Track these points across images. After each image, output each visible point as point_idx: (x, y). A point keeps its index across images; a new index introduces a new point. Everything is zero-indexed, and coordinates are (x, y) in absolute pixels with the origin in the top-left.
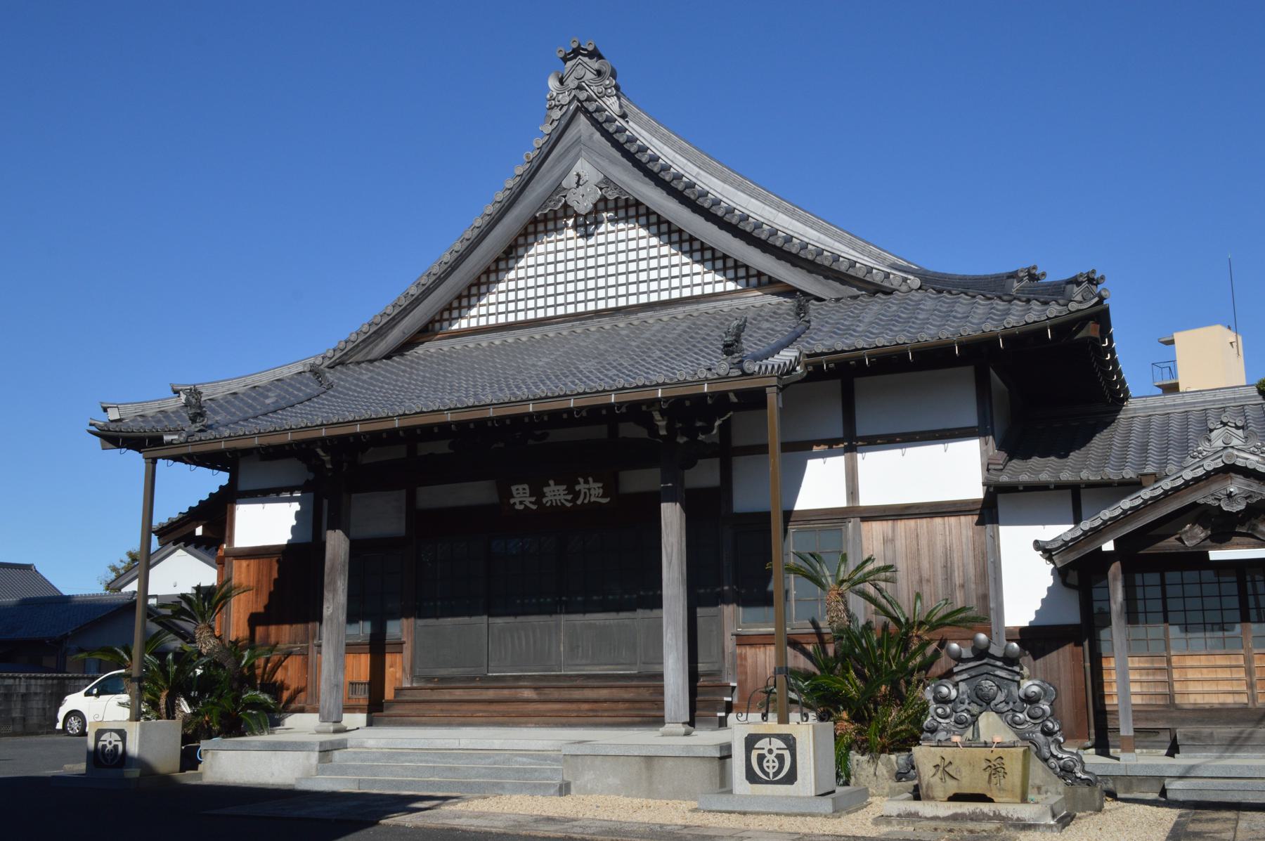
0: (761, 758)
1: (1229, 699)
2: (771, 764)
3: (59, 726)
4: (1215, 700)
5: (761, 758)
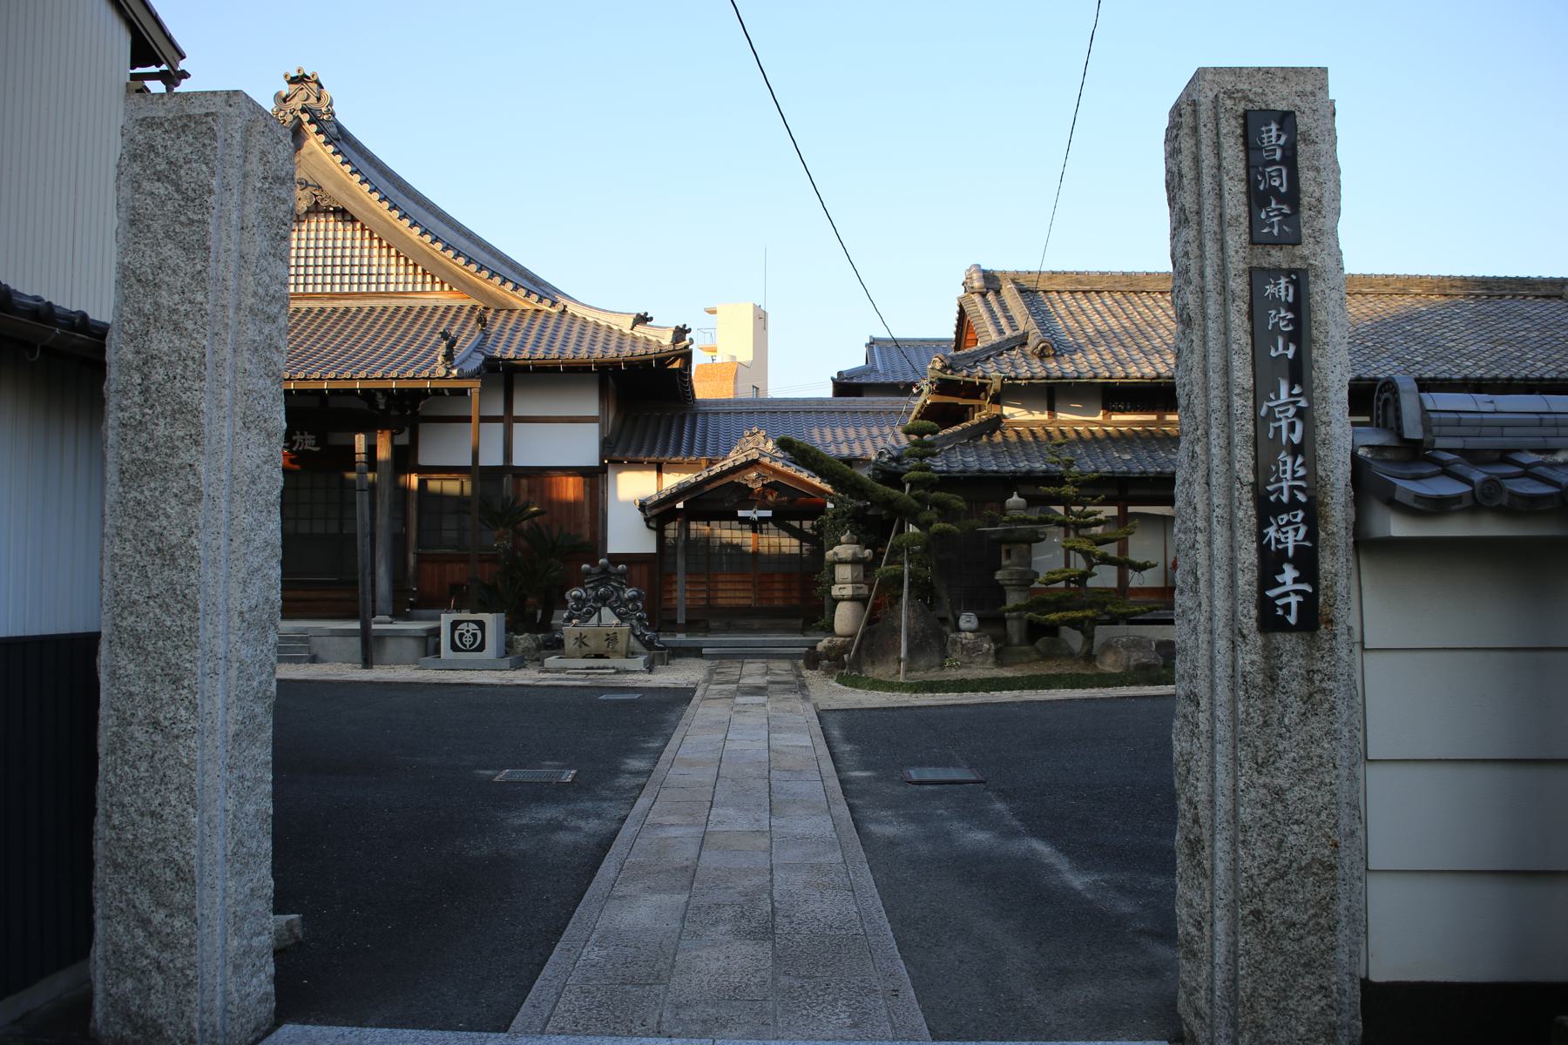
0: (461, 635)
1: (742, 602)
2: (468, 639)
3: (1131, 509)
4: (733, 602)
5: (461, 635)
